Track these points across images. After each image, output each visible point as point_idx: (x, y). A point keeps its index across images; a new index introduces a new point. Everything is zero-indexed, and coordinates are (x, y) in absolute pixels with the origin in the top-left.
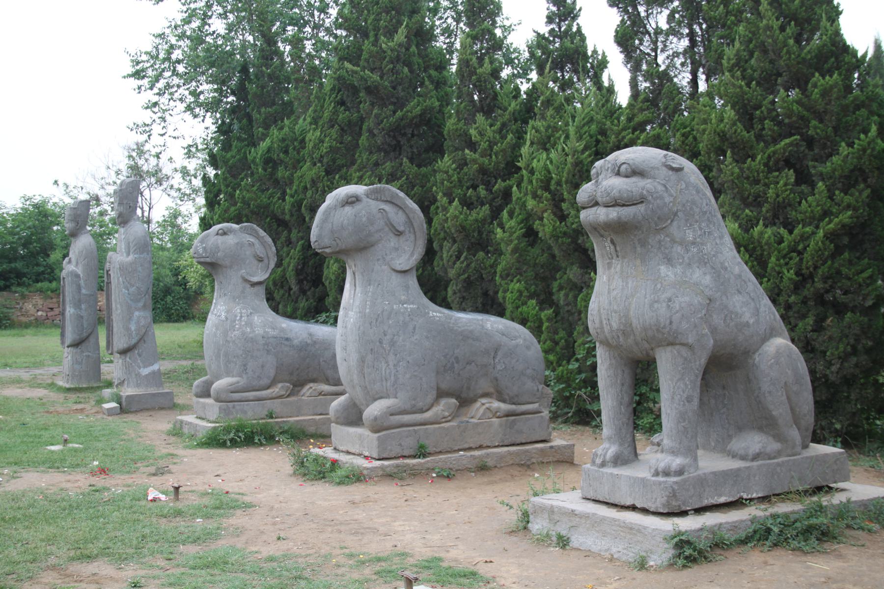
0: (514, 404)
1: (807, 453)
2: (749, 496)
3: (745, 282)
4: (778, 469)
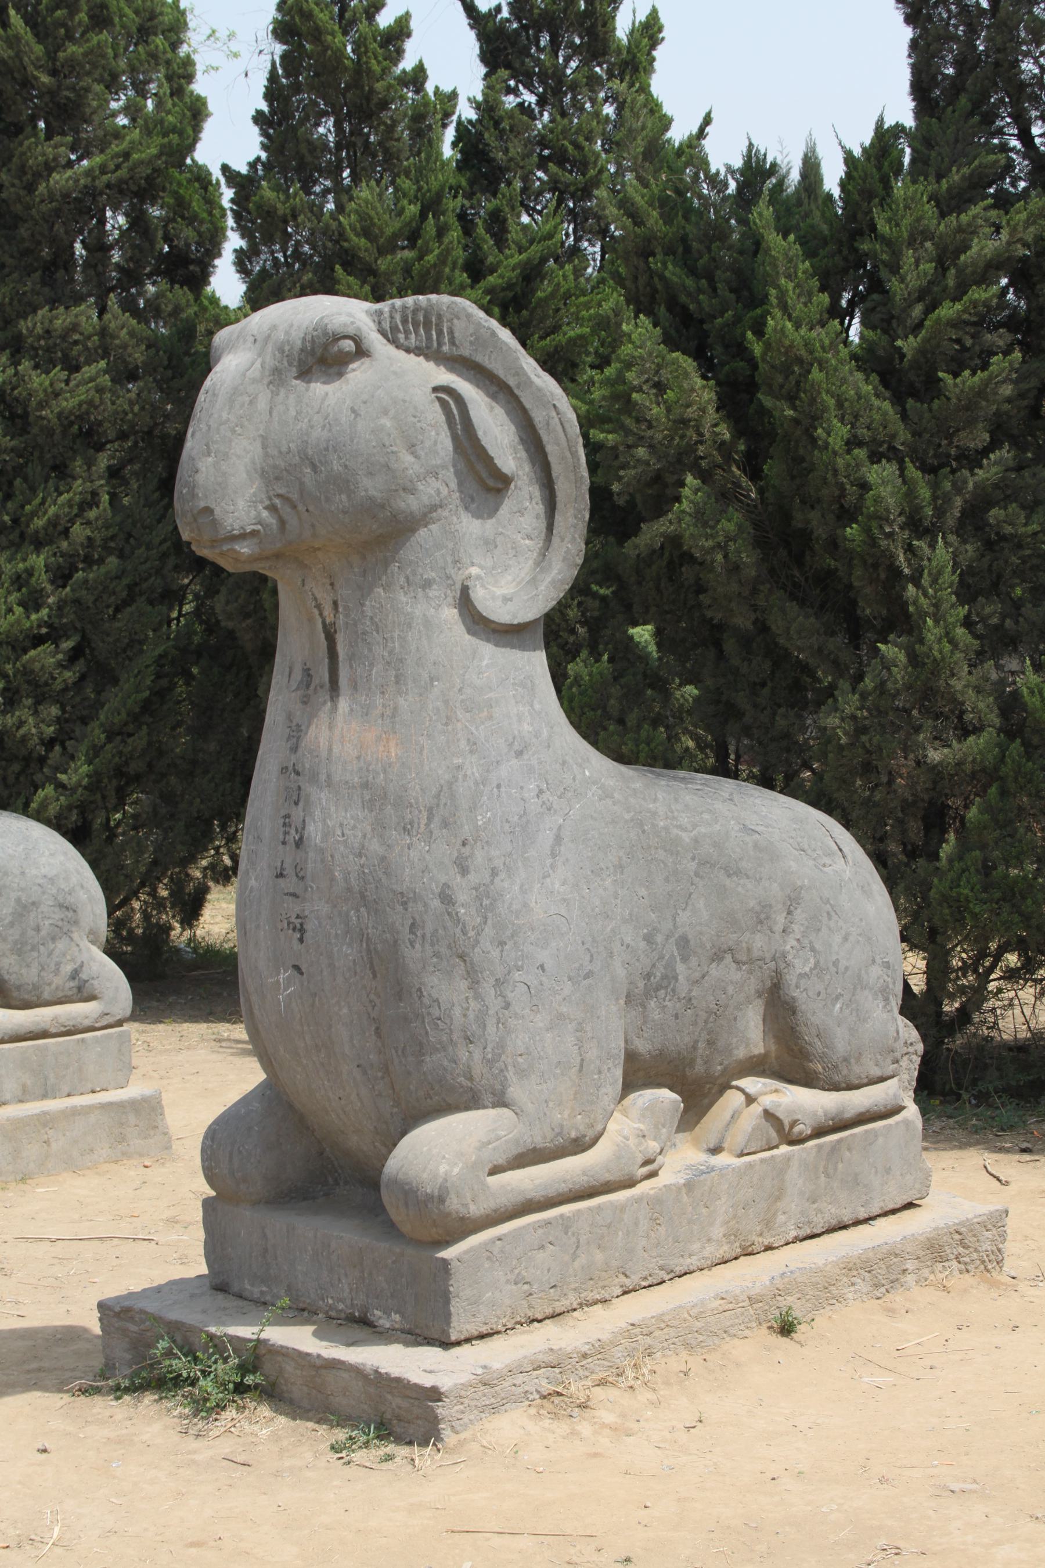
0: (836, 1088)
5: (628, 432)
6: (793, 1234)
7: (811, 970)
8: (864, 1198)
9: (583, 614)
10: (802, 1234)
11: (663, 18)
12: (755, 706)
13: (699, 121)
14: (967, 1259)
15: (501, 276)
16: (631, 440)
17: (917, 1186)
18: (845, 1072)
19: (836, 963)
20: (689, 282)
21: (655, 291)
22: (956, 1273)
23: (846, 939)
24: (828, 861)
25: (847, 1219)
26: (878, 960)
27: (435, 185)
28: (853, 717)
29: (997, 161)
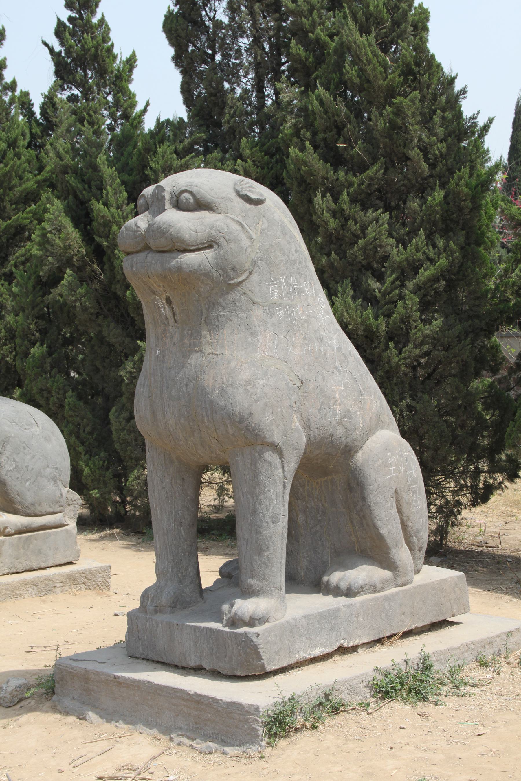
0: (29, 515)
1: (418, 579)
2: (351, 644)
3: (345, 357)
4: (386, 604)
5: (47, 250)
6: (6, 571)
7: (13, 469)
8: (44, 559)
9: (37, 327)
10: (11, 571)
11: (138, 57)
12: (104, 367)
13: (145, 104)
14: (89, 584)
15: (43, 176)
16: (48, 254)
17: (73, 556)
18: (33, 509)
19: (27, 467)
20: (80, 186)
21: (68, 190)
22: (83, 589)
23: (33, 457)
24: (27, 427)
25: (35, 567)
26: (50, 466)
27: (14, 136)
28: (130, 372)
29: (201, 137)
